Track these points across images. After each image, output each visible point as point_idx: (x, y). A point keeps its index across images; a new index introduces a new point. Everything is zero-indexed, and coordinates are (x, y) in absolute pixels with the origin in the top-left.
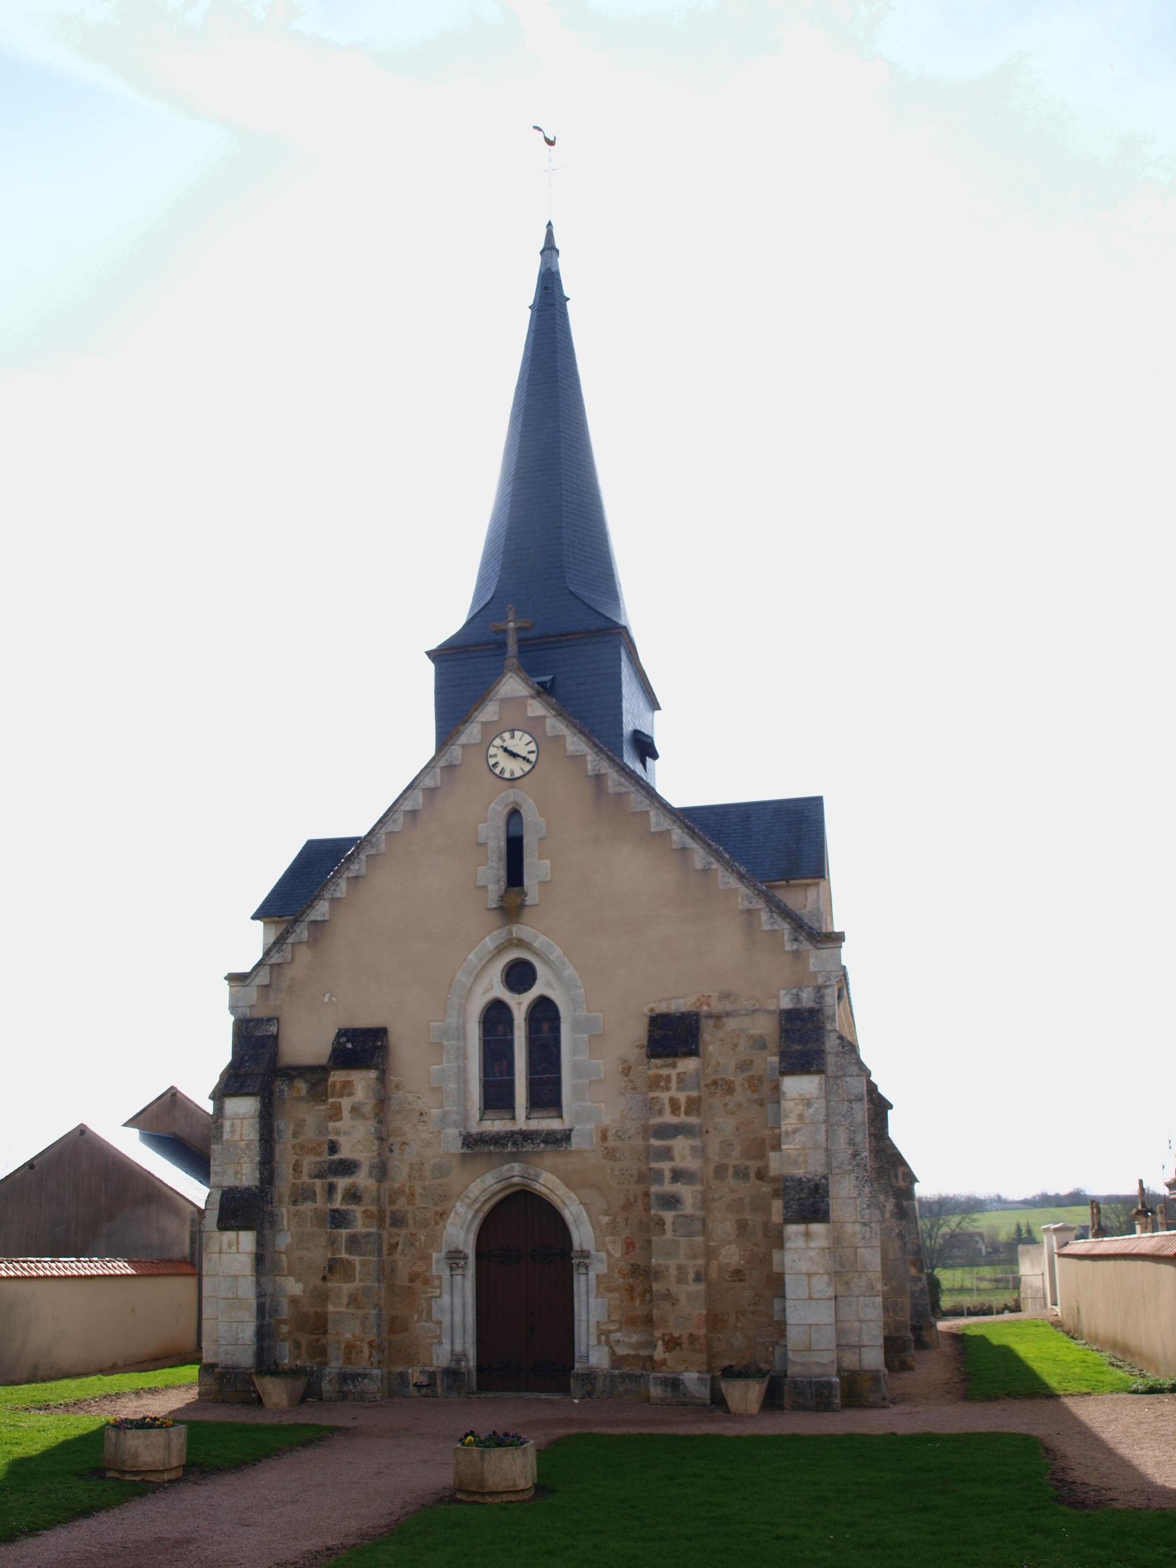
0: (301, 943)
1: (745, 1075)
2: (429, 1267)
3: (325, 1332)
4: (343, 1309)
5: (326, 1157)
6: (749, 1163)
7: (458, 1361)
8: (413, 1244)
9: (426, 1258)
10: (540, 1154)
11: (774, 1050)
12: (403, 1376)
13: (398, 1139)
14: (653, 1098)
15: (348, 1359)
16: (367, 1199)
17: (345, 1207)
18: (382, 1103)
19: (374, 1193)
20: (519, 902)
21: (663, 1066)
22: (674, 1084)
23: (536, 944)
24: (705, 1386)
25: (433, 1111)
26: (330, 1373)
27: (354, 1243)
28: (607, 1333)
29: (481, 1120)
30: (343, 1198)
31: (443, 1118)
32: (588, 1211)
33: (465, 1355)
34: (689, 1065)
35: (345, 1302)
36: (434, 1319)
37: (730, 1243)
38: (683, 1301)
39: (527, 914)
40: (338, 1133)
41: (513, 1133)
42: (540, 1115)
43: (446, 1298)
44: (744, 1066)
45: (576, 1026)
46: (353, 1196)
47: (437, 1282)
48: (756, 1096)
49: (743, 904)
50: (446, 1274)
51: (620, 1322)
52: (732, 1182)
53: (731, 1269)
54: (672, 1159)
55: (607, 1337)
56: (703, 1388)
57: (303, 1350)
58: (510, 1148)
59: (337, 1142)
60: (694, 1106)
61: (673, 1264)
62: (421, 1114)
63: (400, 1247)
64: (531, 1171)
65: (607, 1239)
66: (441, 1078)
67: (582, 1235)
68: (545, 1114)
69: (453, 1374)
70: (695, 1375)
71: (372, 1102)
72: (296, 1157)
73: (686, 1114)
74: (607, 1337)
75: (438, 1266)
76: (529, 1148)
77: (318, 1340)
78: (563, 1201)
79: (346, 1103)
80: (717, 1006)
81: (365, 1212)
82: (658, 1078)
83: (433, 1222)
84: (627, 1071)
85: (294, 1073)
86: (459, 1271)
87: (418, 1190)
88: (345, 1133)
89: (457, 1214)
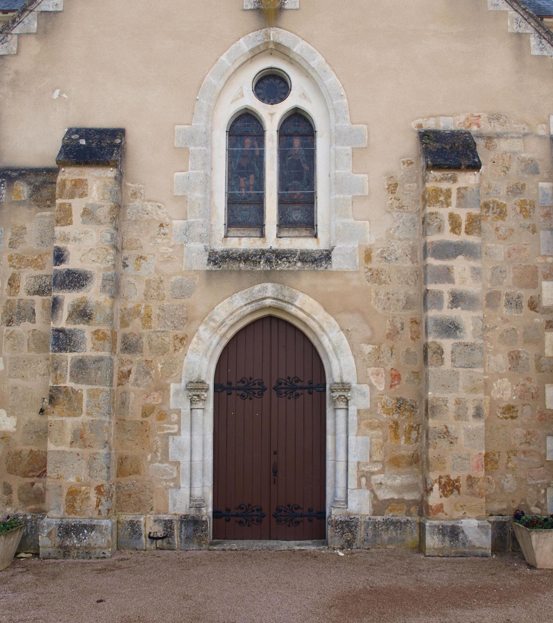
0: (28, 34)
1: (517, 199)
2: (166, 399)
3: (43, 474)
4: (67, 448)
5: (50, 268)
6: (522, 292)
7: (198, 508)
8: (148, 373)
9: (163, 389)
10: (296, 273)
11: (546, 175)
12: (134, 526)
13: (134, 252)
14: (432, 214)
15: (71, 507)
16: (98, 317)
17: (70, 327)
18: (118, 209)
19: (108, 311)
20: (278, 5)
21: (442, 180)
22: (454, 199)
23: (296, 49)
24: (487, 534)
25: (175, 222)
26: (49, 525)
27: (81, 368)
28: (368, 475)
29: (226, 237)
30: (70, 316)
31: (186, 230)
32: (349, 339)
33: (203, 501)
34: (468, 179)
35: (69, 439)
36: (171, 459)
37: (501, 377)
38: (462, 439)
39: (286, 18)
40: (66, 239)
41: (263, 252)
42: (291, 233)
43: (185, 436)
44: (517, 190)
45: (337, 137)
46: (82, 313)
47: (175, 417)
48: (528, 222)
49: (512, 28)
50: (187, 406)
51: (382, 462)
52: (505, 311)
53: (503, 405)
54: (451, 280)
55: (368, 481)
56: (484, 537)
57: (15, 496)
58: (263, 266)
59: (65, 249)
60: (474, 225)
61: (451, 398)
62: (161, 225)
63: (132, 377)
64: (286, 293)
65: (370, 370)
66: (184, 185)
67: (341, 364)
68: (296, 233)
69: (192, 522)
70: (475, 523)
71: (108, 205)
72: (12, 270)
73: (467, 233)
74: (368, 481)
75: (177, 399)
76: (284, 266)
77: (33, 484)
78: (321, 327)
79: (77, 205)
80: (487, 128)
81: (96, 333)
82: (437, 192)
83: (172, 348)
84: (393, 188)
85: (15, 174)
86: (200, 405)
87: (155, 311)
88: (75, 239)
89: (199, 338)
